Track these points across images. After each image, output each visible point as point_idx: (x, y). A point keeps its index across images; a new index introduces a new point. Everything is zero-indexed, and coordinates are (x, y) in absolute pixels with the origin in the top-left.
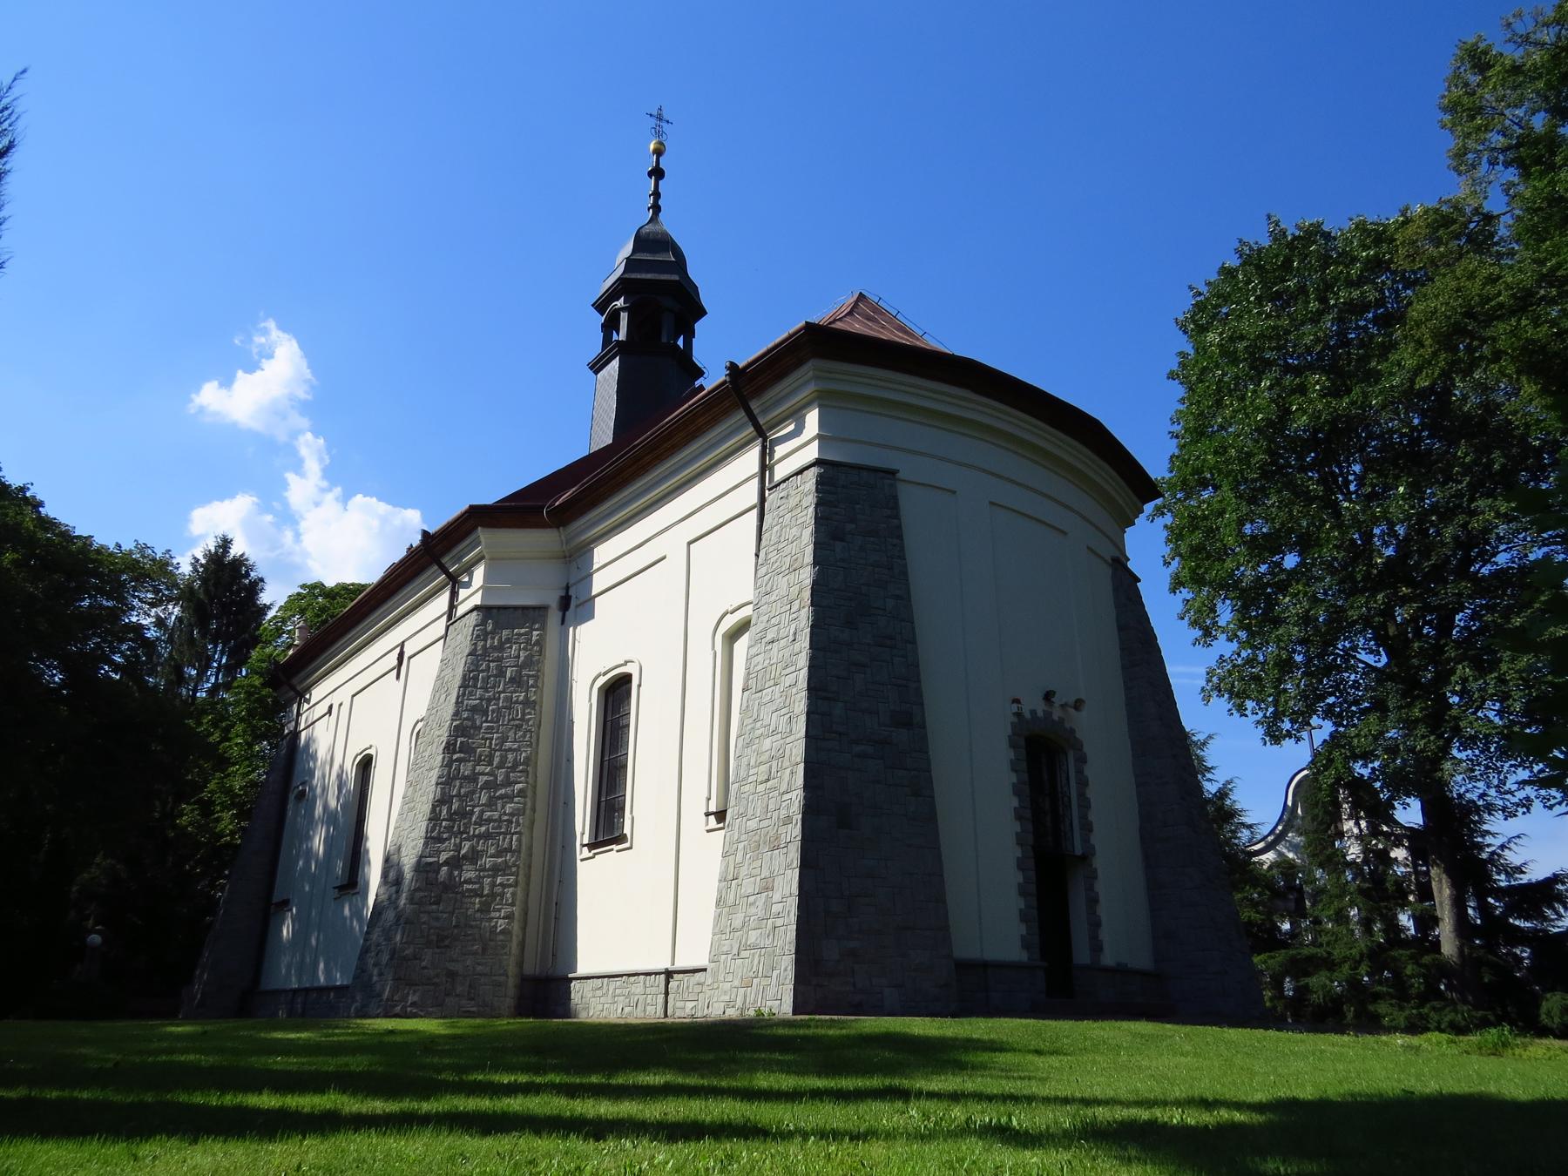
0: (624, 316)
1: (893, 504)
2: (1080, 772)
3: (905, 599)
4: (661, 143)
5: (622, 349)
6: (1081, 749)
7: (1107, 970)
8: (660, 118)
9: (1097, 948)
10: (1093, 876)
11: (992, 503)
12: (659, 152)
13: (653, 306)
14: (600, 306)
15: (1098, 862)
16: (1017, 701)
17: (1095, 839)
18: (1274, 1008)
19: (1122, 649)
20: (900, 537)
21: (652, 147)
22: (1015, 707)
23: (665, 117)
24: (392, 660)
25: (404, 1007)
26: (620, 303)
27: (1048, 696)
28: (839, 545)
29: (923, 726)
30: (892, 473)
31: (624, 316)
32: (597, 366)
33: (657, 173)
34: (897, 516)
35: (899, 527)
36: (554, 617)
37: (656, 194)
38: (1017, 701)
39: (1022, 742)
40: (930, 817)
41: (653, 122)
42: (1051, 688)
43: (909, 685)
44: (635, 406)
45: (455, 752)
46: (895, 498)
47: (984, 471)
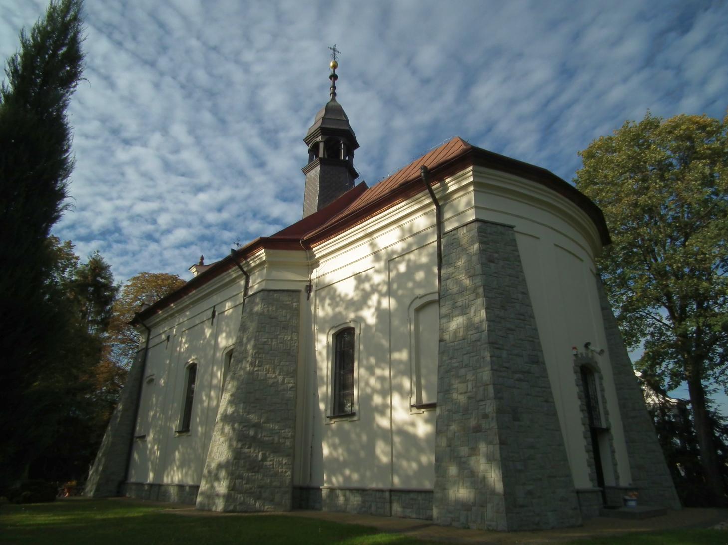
0: (322, 146)
1: (514, 243)
2: (601, 384)
3: (525, 293)
4: (336, 62)
5: (323, 162)
6: (600, 372)
7: (621, 489)
8: (335, 50)
9: (617, 478)
10: (611, 439)
11: (556, 245)
12: (335, 67)
13: (333, 143)
14: (307, 141)
15: (613, 431)
16: (574, 348)
17: (611, 421)
18: (243, 415)
19: (604, 320)
20: (520, 261)
21: (332, 64)
22: (574, 352)
23: (338, 49)
24: (209, 313)
25: (235, 506)
26: (320, 139)
27: (587, 345)
28: (493, 265)
29: (544, 363)
30: (511, 227)
31: (322, 146)
32: (306, 171)
33: (334, 77)
34: (517, 250)
35: (519, 256)
36: (304, 295)
37: (334, 87)
38: (574, 348)
39: (579, 370)
40: (555, 414)
41: (332, 51)
42: (588, 341)
43: (534, 340)
44: (327, 188)
45: (255, 366)
46: (515, 240)
47: (552, 228)
